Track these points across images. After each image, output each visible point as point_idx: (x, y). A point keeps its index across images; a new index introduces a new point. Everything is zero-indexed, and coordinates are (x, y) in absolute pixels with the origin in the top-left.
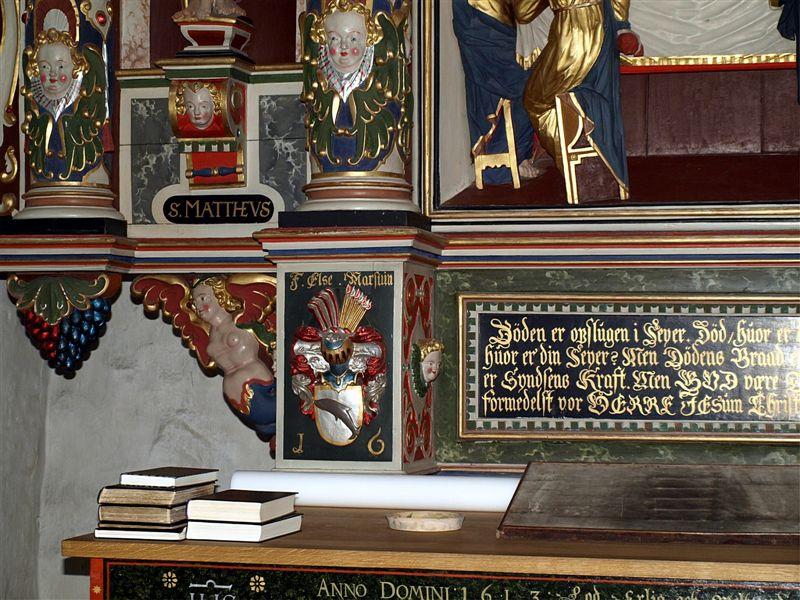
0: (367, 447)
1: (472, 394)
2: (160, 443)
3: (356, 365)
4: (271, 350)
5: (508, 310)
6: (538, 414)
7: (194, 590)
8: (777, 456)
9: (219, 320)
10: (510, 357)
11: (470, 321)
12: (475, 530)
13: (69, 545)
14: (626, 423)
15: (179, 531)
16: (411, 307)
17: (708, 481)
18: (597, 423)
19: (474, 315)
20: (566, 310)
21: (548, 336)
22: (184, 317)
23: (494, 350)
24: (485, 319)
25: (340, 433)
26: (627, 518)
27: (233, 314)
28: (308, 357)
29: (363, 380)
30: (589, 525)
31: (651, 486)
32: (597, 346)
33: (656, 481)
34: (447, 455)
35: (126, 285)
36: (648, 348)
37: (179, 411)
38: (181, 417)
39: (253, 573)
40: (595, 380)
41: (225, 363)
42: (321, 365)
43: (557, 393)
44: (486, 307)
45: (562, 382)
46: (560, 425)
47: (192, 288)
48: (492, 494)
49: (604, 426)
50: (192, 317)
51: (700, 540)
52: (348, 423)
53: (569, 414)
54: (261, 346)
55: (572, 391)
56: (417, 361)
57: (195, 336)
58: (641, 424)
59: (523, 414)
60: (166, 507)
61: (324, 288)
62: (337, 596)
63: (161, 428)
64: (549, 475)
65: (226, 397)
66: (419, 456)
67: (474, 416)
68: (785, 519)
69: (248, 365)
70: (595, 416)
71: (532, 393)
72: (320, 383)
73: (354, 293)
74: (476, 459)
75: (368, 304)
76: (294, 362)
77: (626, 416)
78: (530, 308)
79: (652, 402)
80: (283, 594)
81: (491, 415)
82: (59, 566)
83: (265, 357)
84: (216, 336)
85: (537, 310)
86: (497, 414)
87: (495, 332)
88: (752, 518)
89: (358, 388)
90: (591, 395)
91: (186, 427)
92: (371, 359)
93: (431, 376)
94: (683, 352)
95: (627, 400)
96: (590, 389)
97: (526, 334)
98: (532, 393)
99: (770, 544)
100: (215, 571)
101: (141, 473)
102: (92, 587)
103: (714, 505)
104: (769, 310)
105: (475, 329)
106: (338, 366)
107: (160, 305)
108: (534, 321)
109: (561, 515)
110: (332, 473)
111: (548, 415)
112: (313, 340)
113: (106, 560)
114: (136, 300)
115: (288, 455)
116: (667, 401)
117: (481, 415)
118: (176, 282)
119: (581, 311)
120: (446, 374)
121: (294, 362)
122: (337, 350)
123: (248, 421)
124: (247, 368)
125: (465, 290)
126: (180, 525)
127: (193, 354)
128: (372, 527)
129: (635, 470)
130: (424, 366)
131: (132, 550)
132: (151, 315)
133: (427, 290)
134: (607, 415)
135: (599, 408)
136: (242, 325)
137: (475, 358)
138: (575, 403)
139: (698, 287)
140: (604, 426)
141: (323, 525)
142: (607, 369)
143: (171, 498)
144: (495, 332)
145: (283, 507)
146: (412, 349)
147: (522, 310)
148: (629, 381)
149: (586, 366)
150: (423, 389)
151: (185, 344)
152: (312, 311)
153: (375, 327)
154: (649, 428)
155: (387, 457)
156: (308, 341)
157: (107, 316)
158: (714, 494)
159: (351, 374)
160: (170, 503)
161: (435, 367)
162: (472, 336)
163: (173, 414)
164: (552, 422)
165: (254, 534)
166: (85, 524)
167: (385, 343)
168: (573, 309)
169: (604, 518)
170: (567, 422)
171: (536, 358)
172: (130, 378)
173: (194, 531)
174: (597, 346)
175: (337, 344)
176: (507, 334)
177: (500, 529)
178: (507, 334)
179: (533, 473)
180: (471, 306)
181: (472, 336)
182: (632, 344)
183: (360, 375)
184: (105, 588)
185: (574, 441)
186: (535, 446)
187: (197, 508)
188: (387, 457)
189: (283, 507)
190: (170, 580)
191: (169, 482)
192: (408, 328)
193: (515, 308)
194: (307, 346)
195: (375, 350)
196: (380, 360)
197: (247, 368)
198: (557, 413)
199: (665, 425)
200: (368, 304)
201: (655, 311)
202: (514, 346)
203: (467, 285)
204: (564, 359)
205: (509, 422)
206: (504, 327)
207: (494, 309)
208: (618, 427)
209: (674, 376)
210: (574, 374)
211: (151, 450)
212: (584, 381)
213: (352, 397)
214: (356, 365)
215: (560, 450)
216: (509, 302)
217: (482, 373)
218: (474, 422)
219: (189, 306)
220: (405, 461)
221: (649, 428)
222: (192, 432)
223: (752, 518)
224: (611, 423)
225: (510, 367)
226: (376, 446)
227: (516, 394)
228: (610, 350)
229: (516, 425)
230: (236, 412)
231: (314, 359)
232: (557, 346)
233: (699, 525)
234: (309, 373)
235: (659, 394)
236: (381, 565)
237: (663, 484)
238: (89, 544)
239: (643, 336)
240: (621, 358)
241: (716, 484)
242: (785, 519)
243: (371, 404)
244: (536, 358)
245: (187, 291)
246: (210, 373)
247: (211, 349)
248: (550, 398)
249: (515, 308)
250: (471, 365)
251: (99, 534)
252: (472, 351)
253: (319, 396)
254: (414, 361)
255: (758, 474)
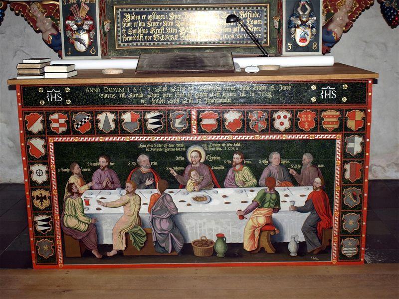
0: (89, 52)
1: (119, 36)
2: (16, 57)
3: (86, 27)
4: (58, 24)
5: (129, 10)
6: (139, 41)
7: (48, 92)
8: (208, 51)
9: (39, 15)
10: (130, 24)
11: (118, 14)
12: (127, 73)
13: (9, 81)
14: (165, 43)
15: (43, 76)
16: (101, 9)
17: (192, 57)
18: (156, 43)
19: (119, 12)
20: (146, 10)
21: (141, 18)
22: (28, 15)
23: (125, 22)
24: (122, 13)
25: (81, 48)
26: (171, 68)
27: (44, 13)
28: (71, 25)
29: (88, 32)
30: (161, 70)
31: (176, 59)
32: (155, 21)
33: (177, 58)
34: (112, 53)
35: (8, 5)
36: (170, 21)
37: (21, 47)
38: (22, 49)
39: (66, 87)
40: (155, 30)
41: (42, 29)
42: (75, 27)
43: (144, 35)
44: (122, 9)
45: (146, 31)
46: (145, 44)
47: (30, 5)
48: (131, 64)
49: (158, 44)
50: (30, 15)
51: (193, 72)
52: (84, 45)
53: (148, 41)
54: (53, 23)
55: (149, 34)
56: (103, 26)
57: (32, 21)
58: (169, 43)
59: (134, 41)
60: (38, 69)
61: (74, 4)
62: (91, 92)
63: (16, 52)
64: (146, 57)
65: (43, 39)
66: (105, 55)
67: (120, 42)
68: (215, 66)
69: (50, 29)
70: (156, 41)
71: (137, 35)
72: (75, 33)
73: (84, 5)
74: (122, 54)
75: (88, 9)
76: (66, 27)
77: (165, 41)
78: (135, 9)
79: (172, 37)
80: (75, 92)
81: (125, 42)
82: (7, 88)
83: (55, 26)
84: (39, 20)
85: (137, 10)
86: (127, 42)
87: (125, 17)
88: (205, 66)
89: (87, 34)
90: (154, 35)
91: (23, 52)
92: (90, 25)
93: (108, 30)
94: (181, 21)
95: (165, 36)
96: (154, 33)
97: (134, 17)
98: (137, 35)
99: (212, 73)
100: (55, 87)
101: (32, 59)
102: (17, 93)
103: (195, 63)
104: (244, 8)
105: (119, 16)
106: (80, 28)
107: (20, 11)
108: (137, 14)
109: (152, 67)
110: (80, 60)
111: (142, 41)
112: (72, 20)
113: (21, 85)
114: (12, 10)
115: (66, 55)
116: (176, 36)
117: (122, 42)
118: (24, 4)
119: (150, 10)
120: (112, 30)
121: (66, 27)
122: (80, 23)
123: (50, 46)
124: (49, 30)
125: (116, 4)
126: (43, 74)
127: (31, 26)
128: (98, 73)
129: (170, 55)
130: (105, 27)
131: (30, 81)
132: (17, 15)
133: (104, 5)
134: (159, 41)
135: (156, 39)
136: (47, 17)
137: (119, 25)
138: (150, 38)
139: (185, 2)
140: (158, 44)
141: (83, 74)
142: (159, 27)
143: (39, 66)
144: (125, 17)
145: (71, 68)
146: (102, 22)
147: (133, 10)
148: (165, 30)
149: (153, 27)
150: (105, 35)
151: (29, 23)
152: (71, 11)
153: (91, 16)
154: (171, 44)
155: (96, 55)
156: (70, 20)
157: (3, 15)
158: (194, 60)
159: (84, 30)
160: (39, 68)
161: (108, 28)
162: (118, 18)
163: (19, 48)
164: (143, 44)
165: (66, 76)
166: (14, 75)
167: (94, 20)
168: (148, 9)
169: (165, 68)
170: (148, 43)
171: (138, 24)
172: (4, 37)
173: (47, 76)
174: (155, 21)
175: (80, 21)
176: (129, 17)
177: (136, 71)
178: (129, 17)
179: (142, 56)
180: (117, 9)
181: (118, 18)
182: (165, 20)
183: (87, 30)
184: (21, 93)
185: (150, 49)
186: (138, 51)
187: (47, 69)
188: (96, 55)
189: (71, 68)
190: (41, 90)
191: (39, 61)
192: (100, 16)
193: (131, 10)
194: (70, 22)
195: (91, 23)
196: (93, 26)
197: (49, 30)
198: (145, 41)
199: (176, 43)
200: (88, 9)
201: (133, 10)
202: (131, 21)
203: (116, 3)
204: (146, 24)
205: (130, 44)
206: (128, 15)
207: (125, 10)
208: (163, 44)
209: (178, 29)
210: (149, 29)
211: (13, 59)
212: (152, 31)
213: (85, 37)
214: (86, 27)
215: (145, 51)
216: (129, 8)
217: (122, 29)
218: (120, 44)
219: (29, 11)
220: (102, 56)
221: (171, 44)
222: (25, 53)
223: (205, 66)
224: (160, 43)
225: (130, 27)
226: (93, 52)
227: (132, 35)
228: (159, 22)
229: (133, 45)
230: (47, 44)
231: (72, 26)
232: (144, 21)
233: (190, 67)
234: (71, 30)
235: (174, 34)
236: (105, 82)
237: (179, 58)
238: (15, 81)
239: (169, 17)
240: (163, 24)
241: (194, 58)
242: (215, 66)
243: (91, 39)
244: (138, 24)
245: (28, 7)
246: (38, 32)
247: (37, 25)
248: (142, 36)
249: (131, 10)
250: (118, 27)
251: (18, 78)
252: (119, 23)
253: (75, 37)
254: (102, 26)
255: (206, 55)
